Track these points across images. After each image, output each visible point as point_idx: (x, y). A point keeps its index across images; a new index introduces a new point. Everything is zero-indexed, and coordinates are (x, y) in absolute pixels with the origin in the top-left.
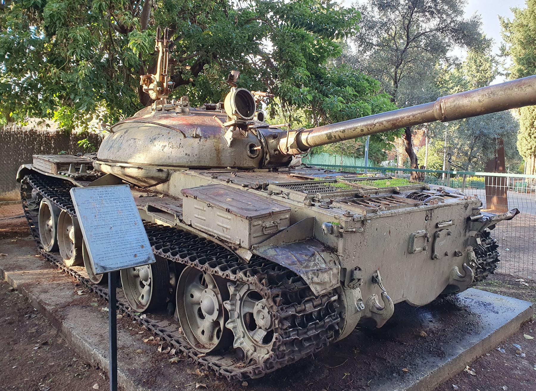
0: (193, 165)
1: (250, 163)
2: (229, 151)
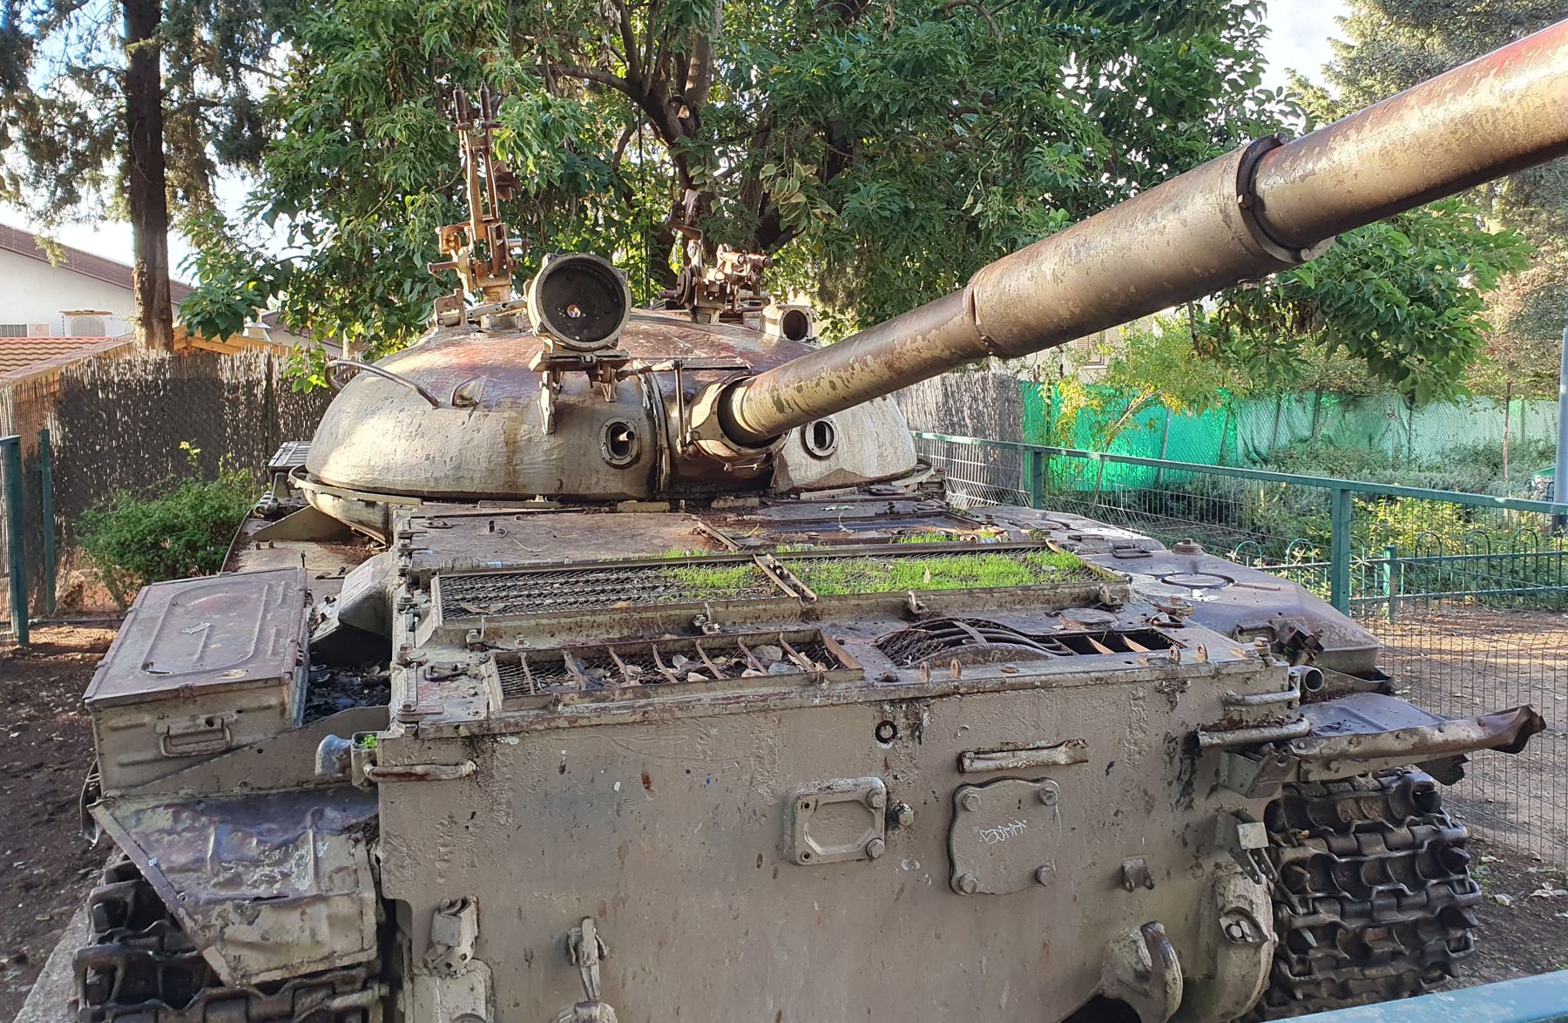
0: (442, 489)
1: (612, 484)
2: (546, 446)
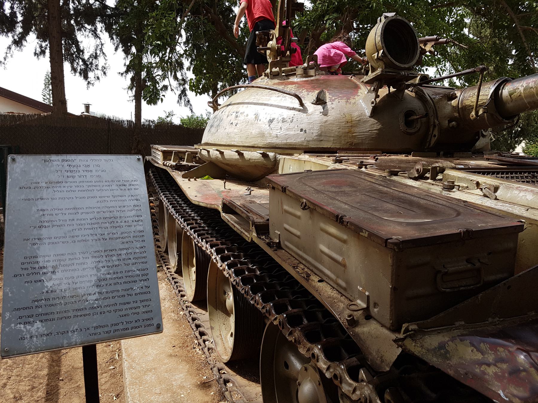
2: (370, 123)
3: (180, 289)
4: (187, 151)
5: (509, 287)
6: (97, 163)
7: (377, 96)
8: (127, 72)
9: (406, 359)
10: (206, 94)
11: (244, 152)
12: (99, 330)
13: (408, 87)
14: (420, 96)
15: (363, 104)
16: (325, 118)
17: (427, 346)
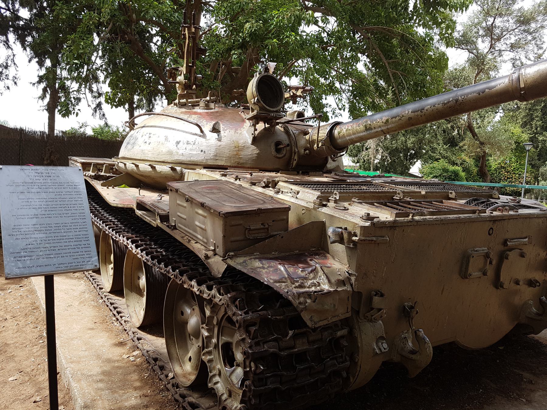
2: (252, 149)
3: (98, 283)
4: (105, 163)
5: (282, 237)
6: (54, 172)
7: (256, 130)
8: (39, 82)
9: (230, 270)
10: (122, 107)
11: (156, 166)
12: (61, 266)
13: (278, 124)
14: (287, 131)
15: (246, 134)
16: (219, 143)
17: (238, 263)
